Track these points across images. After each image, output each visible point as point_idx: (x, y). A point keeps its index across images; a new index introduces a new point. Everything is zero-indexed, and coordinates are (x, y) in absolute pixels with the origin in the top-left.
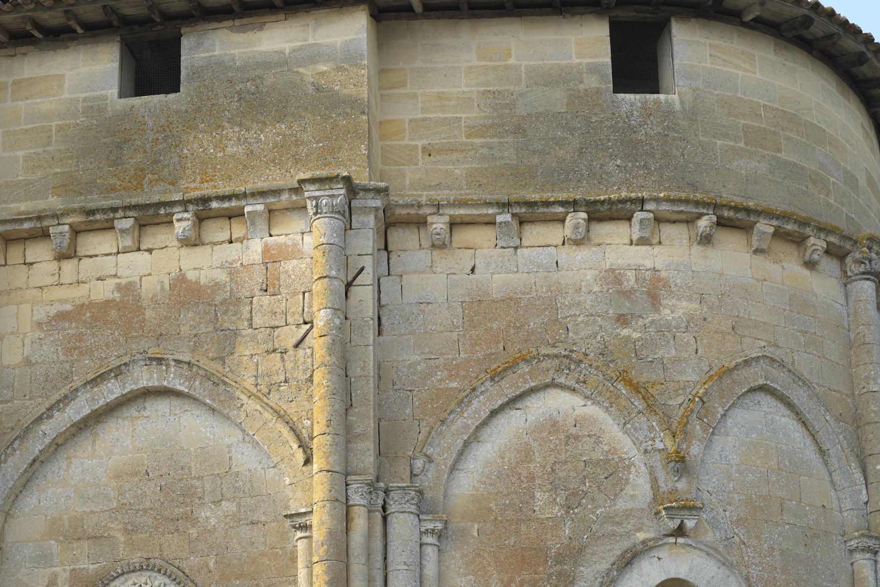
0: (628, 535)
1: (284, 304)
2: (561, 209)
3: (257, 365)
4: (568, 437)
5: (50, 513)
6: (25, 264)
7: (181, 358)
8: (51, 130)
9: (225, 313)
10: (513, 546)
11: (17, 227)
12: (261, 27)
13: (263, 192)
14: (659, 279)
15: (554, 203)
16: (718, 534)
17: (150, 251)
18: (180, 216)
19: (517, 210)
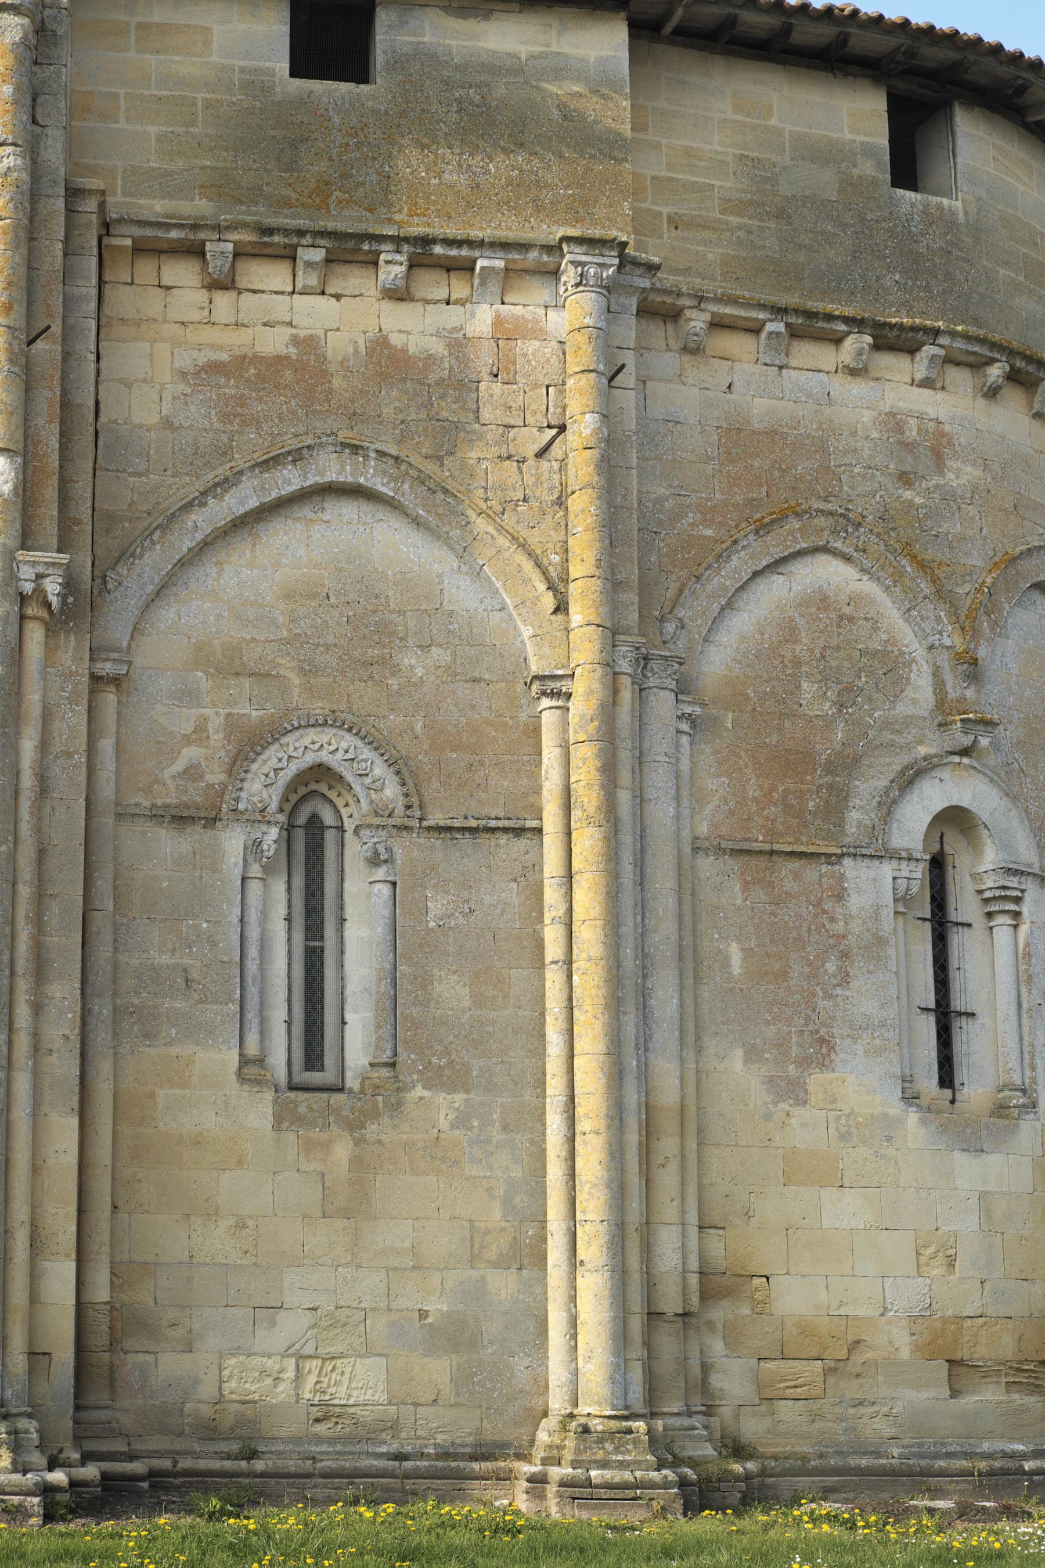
0: (908, 747)
1: (521, 398)
2: (843, 327)
3: (487, 474)
4: (841, 617)
5: (195, 634)
6: (159, 286)
7: (384, 449)
8: (195, 105)
9: (442, 397)
10: (776, 746)
11: (160, 234)
13: (508, 244)
14: (943, 434)
15: (838, 318)
16: (999, 758)
17: (338, 297)
18: (389, 257)
19: (792, 319)
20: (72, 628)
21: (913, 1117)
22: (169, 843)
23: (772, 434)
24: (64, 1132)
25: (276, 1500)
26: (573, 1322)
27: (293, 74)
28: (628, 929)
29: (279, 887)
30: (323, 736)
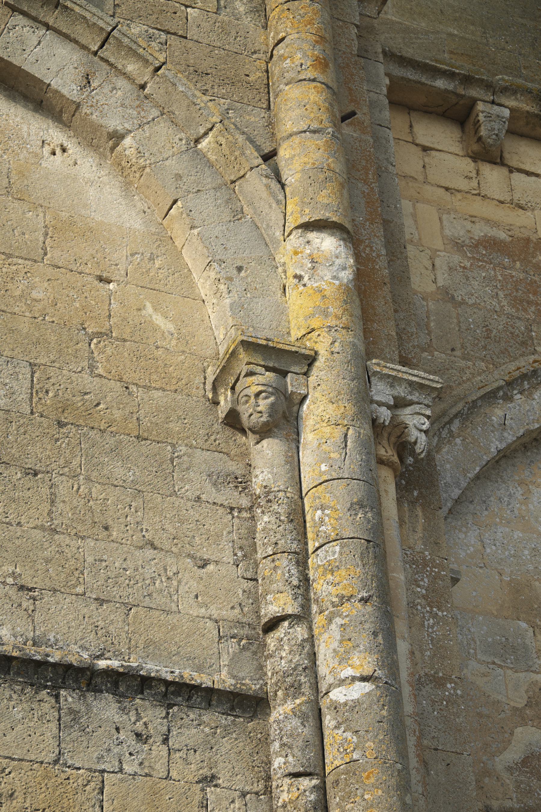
11: (423, 80)
20: (417, 499)
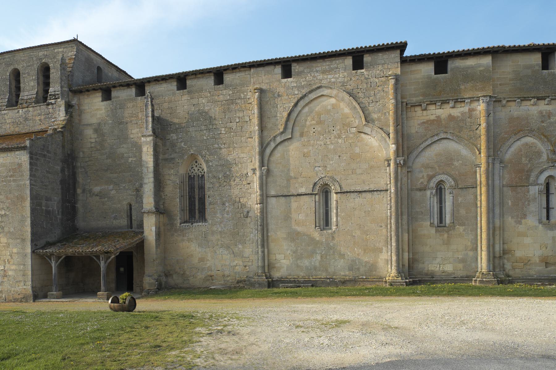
0: (542, 167)
12: (467, 59)
21: (541, 226)
22: (419, 194)
23: (518, 118)
24: (406, 236)
25: (437, 283)
26: (481, 258)
27: (435, 74)
28: (491, 201)
29: (435, 198)
30: (442, 176)
